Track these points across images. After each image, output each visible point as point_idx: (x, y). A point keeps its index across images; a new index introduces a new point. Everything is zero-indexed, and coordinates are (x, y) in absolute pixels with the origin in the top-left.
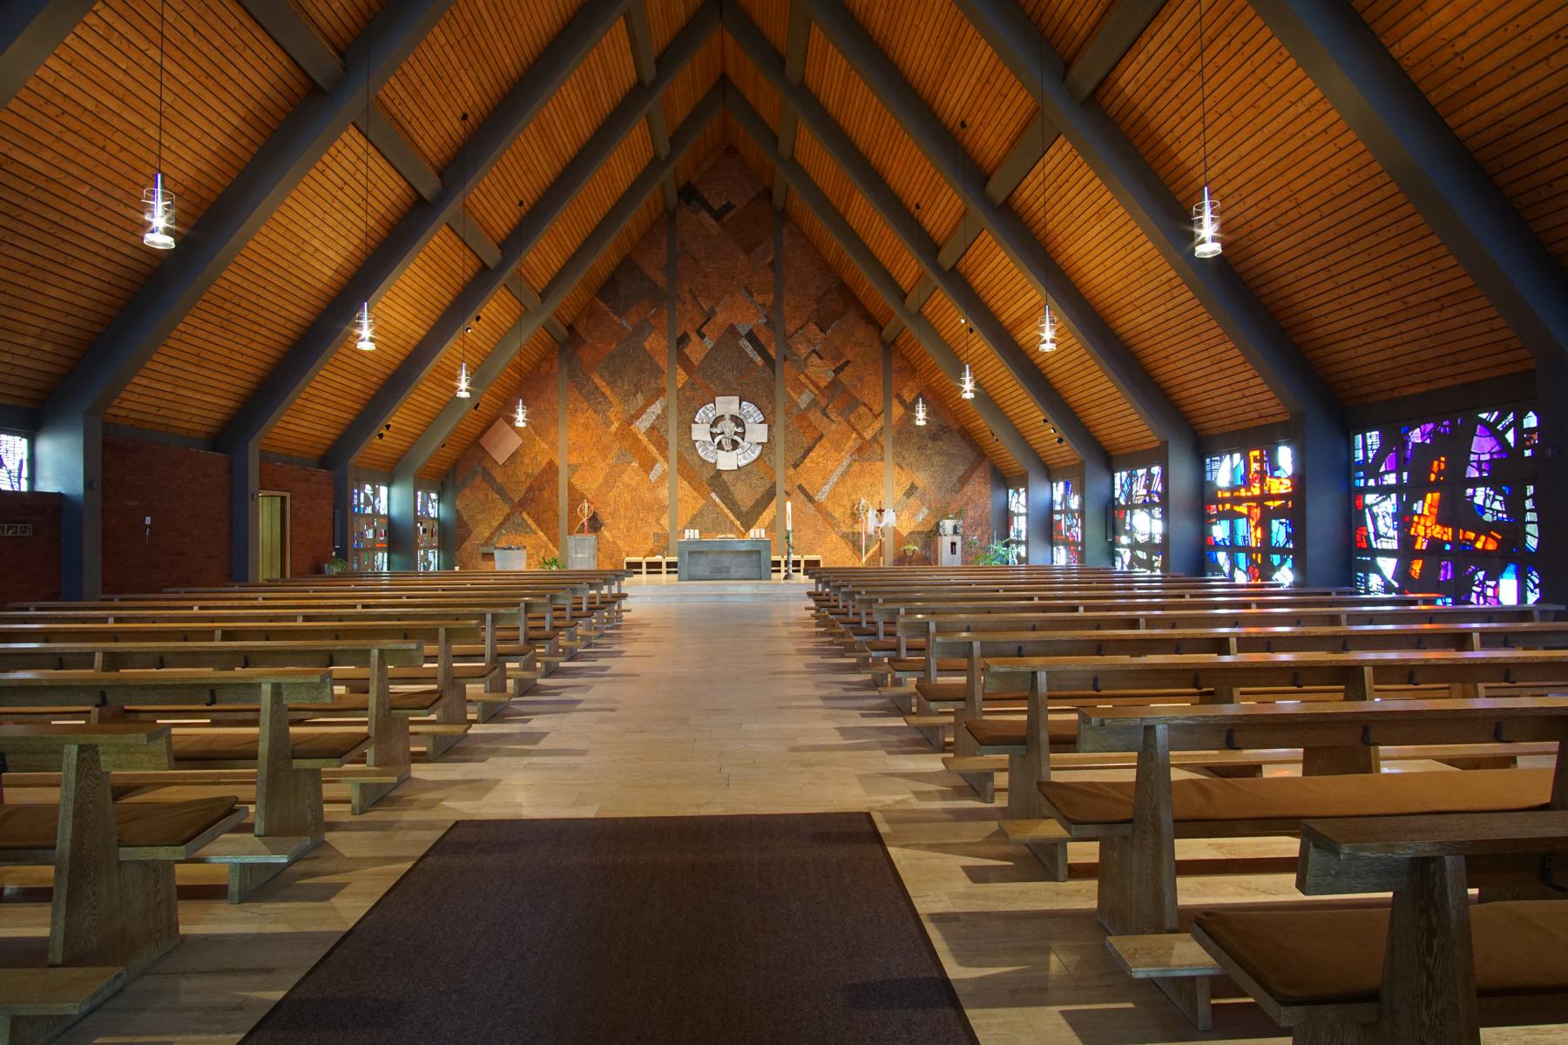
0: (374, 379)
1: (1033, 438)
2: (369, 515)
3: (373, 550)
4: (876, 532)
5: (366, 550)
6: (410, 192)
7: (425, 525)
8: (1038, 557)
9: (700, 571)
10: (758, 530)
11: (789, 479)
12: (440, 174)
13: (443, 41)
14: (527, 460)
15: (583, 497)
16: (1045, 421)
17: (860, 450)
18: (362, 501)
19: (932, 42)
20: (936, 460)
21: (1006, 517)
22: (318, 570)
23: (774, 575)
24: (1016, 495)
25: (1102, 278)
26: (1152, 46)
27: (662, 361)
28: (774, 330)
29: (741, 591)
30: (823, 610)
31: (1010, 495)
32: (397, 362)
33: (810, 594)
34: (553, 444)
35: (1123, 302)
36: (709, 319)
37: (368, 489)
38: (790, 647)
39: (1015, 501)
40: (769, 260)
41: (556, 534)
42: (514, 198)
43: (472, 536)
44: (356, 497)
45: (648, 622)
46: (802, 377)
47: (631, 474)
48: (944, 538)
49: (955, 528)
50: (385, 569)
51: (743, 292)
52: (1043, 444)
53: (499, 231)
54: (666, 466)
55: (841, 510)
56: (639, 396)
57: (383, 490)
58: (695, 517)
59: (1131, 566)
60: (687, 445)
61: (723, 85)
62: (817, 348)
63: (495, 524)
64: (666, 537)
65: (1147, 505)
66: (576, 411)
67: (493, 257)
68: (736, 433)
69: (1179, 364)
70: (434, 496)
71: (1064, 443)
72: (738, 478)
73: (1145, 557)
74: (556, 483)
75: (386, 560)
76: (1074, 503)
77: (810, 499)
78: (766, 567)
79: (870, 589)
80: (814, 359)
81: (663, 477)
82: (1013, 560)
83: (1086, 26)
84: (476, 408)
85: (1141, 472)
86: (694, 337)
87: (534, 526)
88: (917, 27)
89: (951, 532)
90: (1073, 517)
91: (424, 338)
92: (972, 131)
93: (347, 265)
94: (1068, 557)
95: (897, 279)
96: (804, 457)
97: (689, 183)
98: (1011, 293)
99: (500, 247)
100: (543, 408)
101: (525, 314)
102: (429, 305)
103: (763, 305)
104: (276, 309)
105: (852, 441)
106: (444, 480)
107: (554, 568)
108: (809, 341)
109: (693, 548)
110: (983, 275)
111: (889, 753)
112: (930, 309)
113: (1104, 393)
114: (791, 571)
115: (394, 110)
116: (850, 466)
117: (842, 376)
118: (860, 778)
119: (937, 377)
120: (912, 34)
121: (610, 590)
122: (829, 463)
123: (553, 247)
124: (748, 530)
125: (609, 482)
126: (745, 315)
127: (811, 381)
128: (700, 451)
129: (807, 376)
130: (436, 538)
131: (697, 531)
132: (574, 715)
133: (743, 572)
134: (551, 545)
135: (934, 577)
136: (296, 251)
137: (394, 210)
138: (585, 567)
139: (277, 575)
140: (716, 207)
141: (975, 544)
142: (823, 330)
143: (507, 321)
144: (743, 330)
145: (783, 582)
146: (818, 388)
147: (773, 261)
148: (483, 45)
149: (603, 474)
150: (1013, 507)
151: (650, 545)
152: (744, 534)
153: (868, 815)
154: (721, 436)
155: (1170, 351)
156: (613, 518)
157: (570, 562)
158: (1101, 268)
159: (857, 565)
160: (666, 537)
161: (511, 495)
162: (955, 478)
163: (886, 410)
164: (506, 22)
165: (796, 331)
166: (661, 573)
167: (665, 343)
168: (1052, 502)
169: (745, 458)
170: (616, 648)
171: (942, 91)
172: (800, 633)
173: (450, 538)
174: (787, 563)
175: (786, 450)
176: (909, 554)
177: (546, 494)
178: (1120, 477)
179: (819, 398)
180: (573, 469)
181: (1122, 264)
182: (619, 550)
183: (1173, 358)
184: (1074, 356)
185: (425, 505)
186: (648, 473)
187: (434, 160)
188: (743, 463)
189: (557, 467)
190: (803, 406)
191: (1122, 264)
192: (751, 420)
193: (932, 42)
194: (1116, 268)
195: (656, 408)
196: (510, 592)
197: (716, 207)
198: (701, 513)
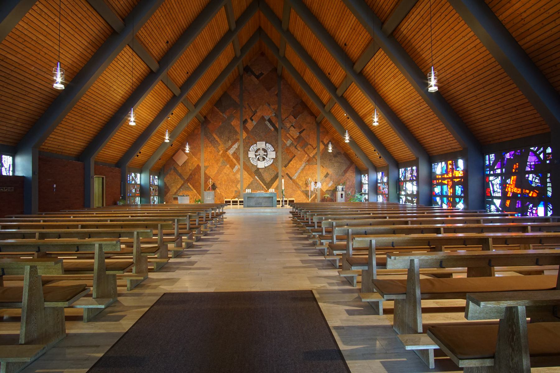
0: (135, 136)
1: (370, 157)
2: (133, 184)
3: (135, 196)
4: (314, 190)
5: (132, 196)
6: (148, 69)
7: (153, 188)
8: (372, 199)
9: (251, 204)
10: (272, 190)
11: (283, 171)
12: (159, 62)
13: (160, 15)
14: (190, 164)
15: (209, 177)
16: (375, 150)
17: (308, 161)
18: (131, 179)
19: (334, 15)
20: (336, 164)
21: (361, 185)
22: (115, 204)
23: (278, 206)
24: (364, 177)
25: (395, 99)
26: (413, 16)
27: (238, 129)
28: (278, 118)
29: (267, 212)
30: (295, 218)
31: (362, 177)
32: (143, 129)
33: (290, 212)
34: (199, 159)
35: (403, 108)
36: (254, 114)
37: (133, 174)
38: (284, 231)
39: (364, 179)
40: (276, 93)
41: (200, 191)
42: (185, 71)
43: (170, 191)
44: (129, 177)
45: (232, 222)
46: (288, 135)
47: (227, 169)
48: (339, 192)
49: (342, 189)
50: (139, 203)
51: (267, 104)
52: (374, 159)
53: (179, 82)
54: (239, 167)
55: (302, 182)
56: (230, 142)
57: (138, 175)
58: (249, 185)
59: (405, 202)
60: (247, 159)
61: (260, 30)
62: (293, 125)
63: (178, 187)
64: (239, 192)
65: (411, 181)
66: (207, 147)
67: (177, 92)
68: (264, 155)
69: (423, 130)
70: (156, 177)
71: (381, 158)
72: (265, 171)
73: (410, 199)
74: (200, 173)
75: (139, 200)
76: (385, 180)
77: (291, 178)
78: (275, 202)
79: (312, 211)
80: (292, 128)
81: (239, 170)
82: (363, 200)
83: (389, 9)
84: (171, 146)
85: (409, 169)
86: (249, 121)
87: (192, 188)
88: (329, 10)
89: (341, 190)
90: (385, 185)
91: (153, 121)
92: (348, 47)
93: (126, 95)
94: (383, 199)
95: (322, 100)
96: (289, 163)
97: (247, 66)
98: (362, 105)
99: (180, 88)
100: (195, 146)
101: (189, 112)
102: (154, 109)
103: (274, 109)
104: (100, 111)
105: (306, 158)
106: (160, 171)
107: (199, 203)
108: (290, 122)
109: (249, 196)
110: (353, 98)
111: (319, 269)
112: (333, 111)
113: (396, 140)
114: (284, 204)
115: (142, 40)
116: (305, 166)
117: (302, 134)
118: (308, 277)
119: (336, 135)
120: (327, 12)
121: (219, 211)
122: (297, 165)
123: (199, 88)
124: (268, 189)
125: (219, 172)
126: (268, 113)
127: (291, 136)
128: (251, 161)
129: (289, 135)
130: (157, 192)
131: (250, 190)
132: (206, 255)
133: (266, 204)
134: (198, 195)
135: (335, 206)
136: (107, 90)
137: (142, 75)
138: (210, 203)
139: (100, 205)
140: (257, 74)
141: (349, 194)
142: (295, 118)
143: (182, 115)
144: (267, 118)
145: (281, 208)
146: (294, 139)
147: (277, 93)
148: (174, 16)
149: (217, 169)
150: (363, 181)
151: (233, 195)
152: (267, 191)
153: (311, 291)
154: (259, 156)
155: (420, 125)
156: (220, 185)
157: (205, 201)
158: (395, 96)
159: (307, 202)
160: (239, 192)
161: (184, 177)
162: (343, 171)
163: (318, 147)
164: (182, 8)
165: (286, 118)
166: (237, 205)
167: (239, 122)
168: (377, 179)
169: (267, 164)
170: (221, 231)
171: (338, 32)
172: (286, 226)
173: (162, 192)
174: (282, 201)
175: (282, 161)
176: (326, 198)
177: (196, 177)
178: (402, 170)
179: (294, 142)
180: (206, 167)
181: (402, 94)
182: (222, 197)
183: (420, 128)
184: (385, 127)
185: (153, 180)
186: (233, 169)
187: (156, 57)
188: (267, 165)
189: (200, 167)
190: (288, 145)
191: (402, 94)
192: (269, 150)
193: (334, 15)
194: (401, 95)
195: (236, 146)
196: (183, 211)
197: (257, 74)
198: (252, 183)
